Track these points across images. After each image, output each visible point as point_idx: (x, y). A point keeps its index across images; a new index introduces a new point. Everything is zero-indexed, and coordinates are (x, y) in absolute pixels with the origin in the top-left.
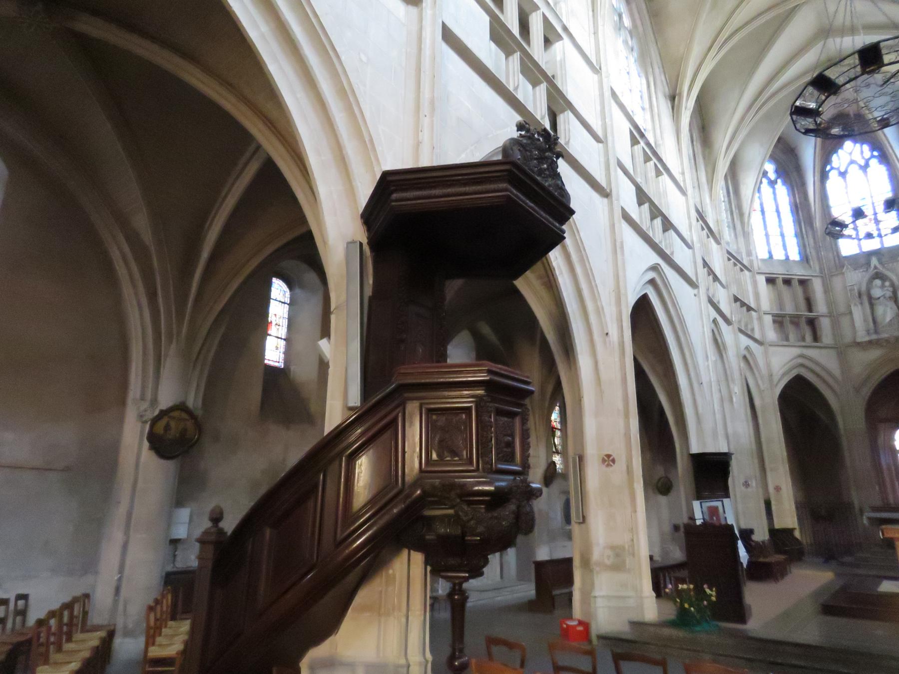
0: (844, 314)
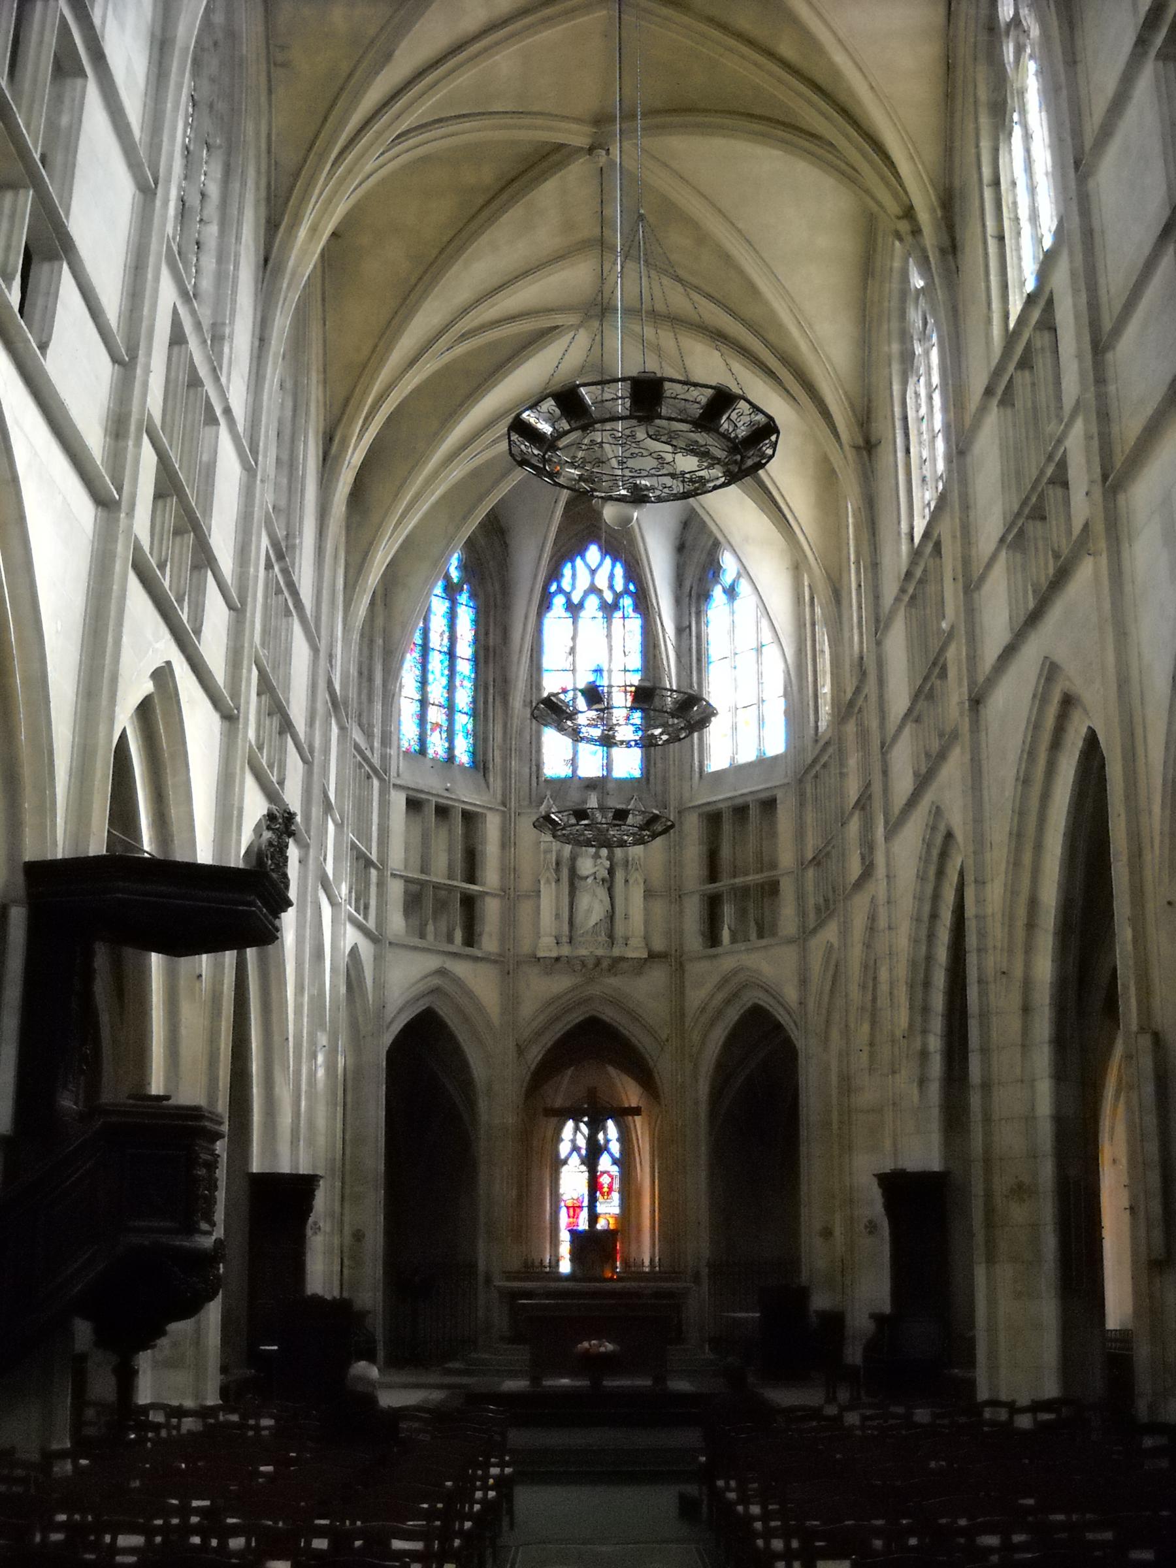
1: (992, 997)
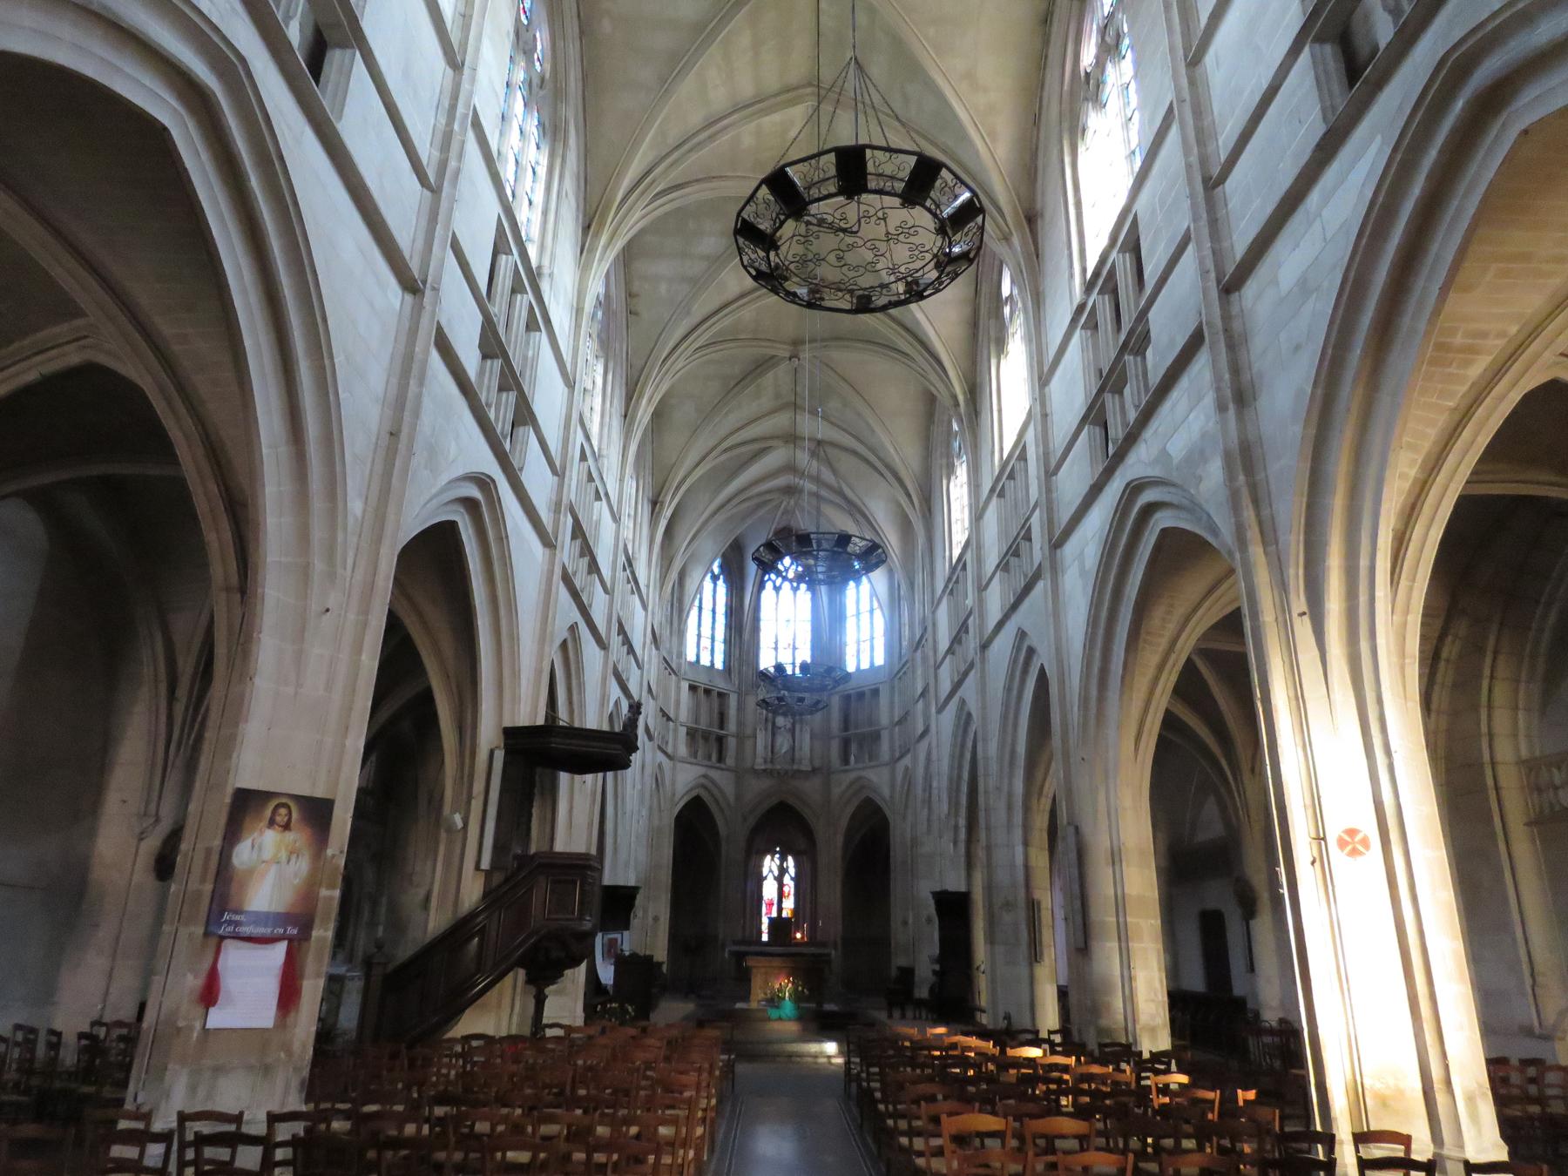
0: (749, 737)
1: (991, 801)
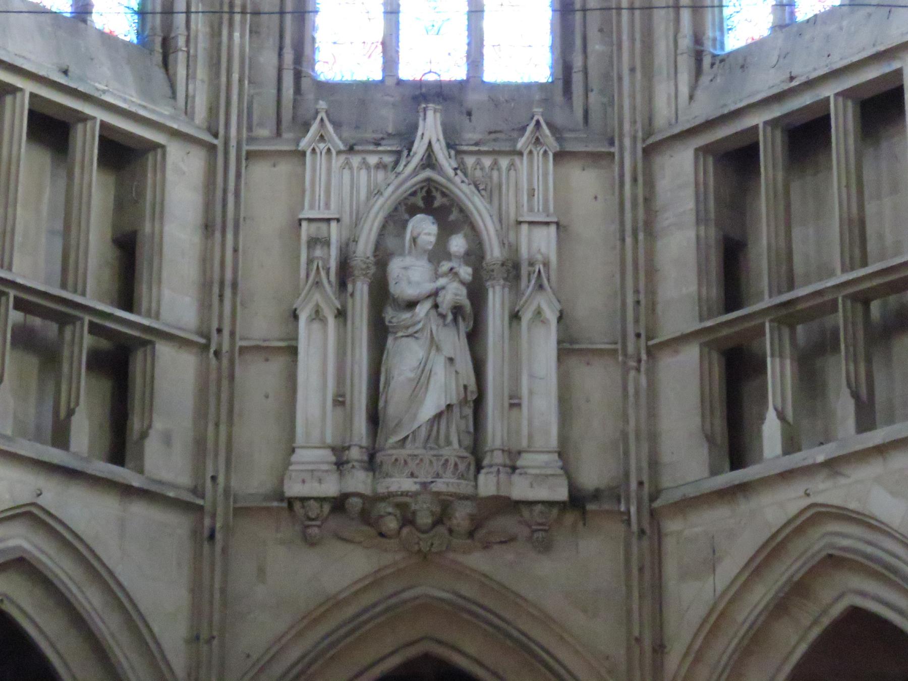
0: (264, 351)
